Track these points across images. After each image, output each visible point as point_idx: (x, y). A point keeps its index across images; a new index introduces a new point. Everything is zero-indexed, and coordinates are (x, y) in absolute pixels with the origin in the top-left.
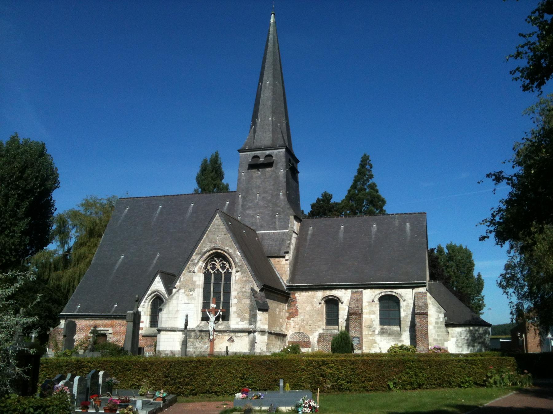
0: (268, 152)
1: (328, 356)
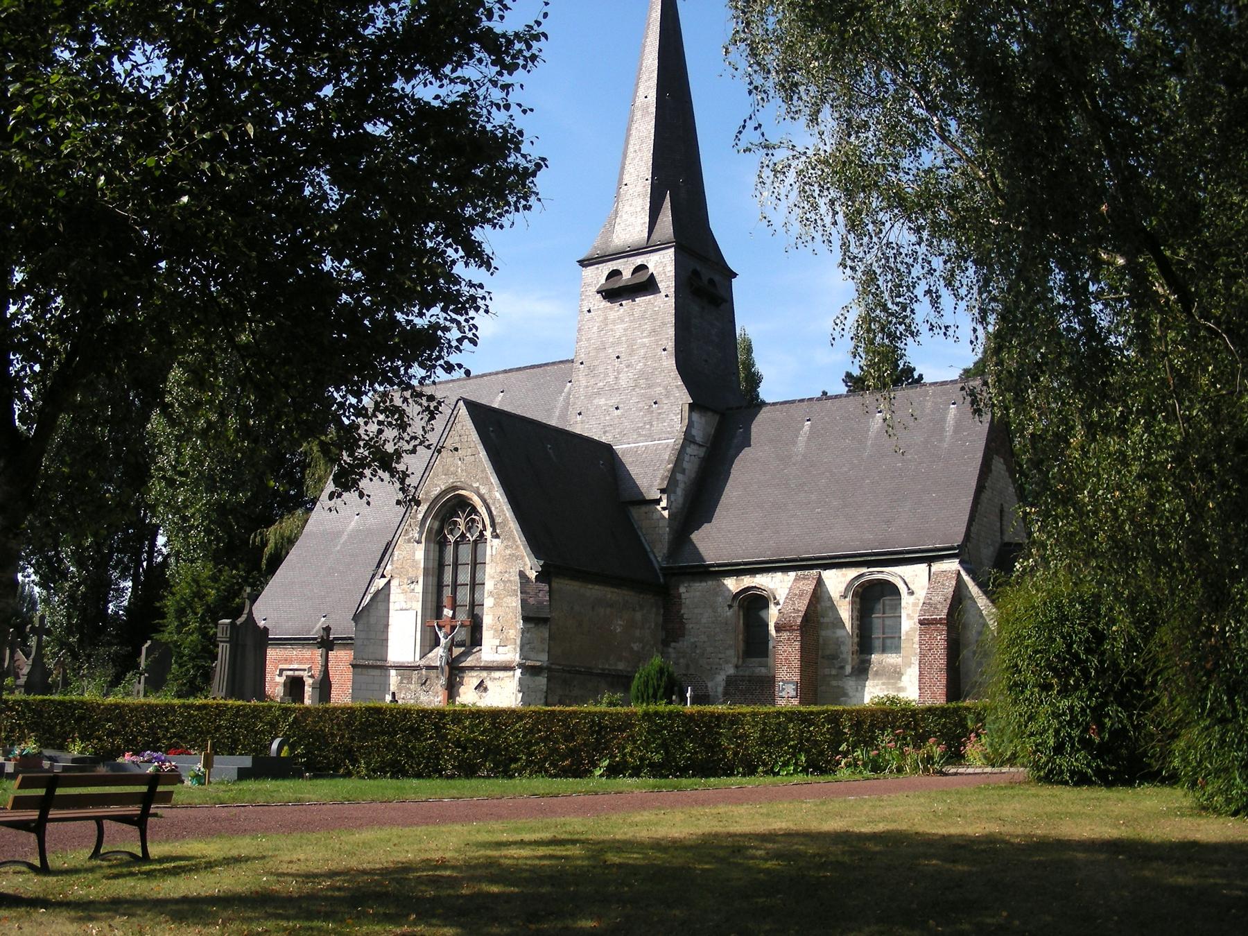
0: (639, 260)
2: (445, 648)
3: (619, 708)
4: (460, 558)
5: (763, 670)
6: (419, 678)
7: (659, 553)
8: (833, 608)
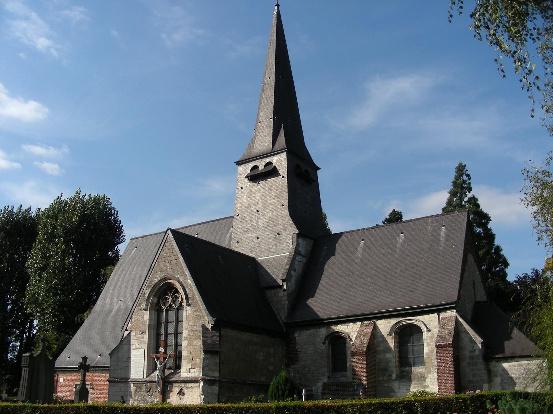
0: (268, 160)
1: (72, 402)
2: (160, 370)
4: (169, 318)
5: (344, 379)
7: (283, 315)
8: (384, 340)
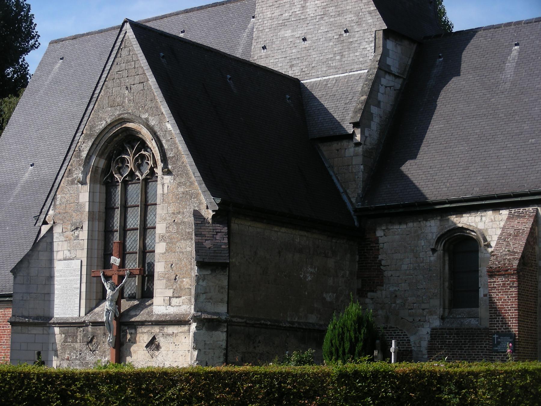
2: (111, 301)
3: (307, 366)
6: (85, 335)
